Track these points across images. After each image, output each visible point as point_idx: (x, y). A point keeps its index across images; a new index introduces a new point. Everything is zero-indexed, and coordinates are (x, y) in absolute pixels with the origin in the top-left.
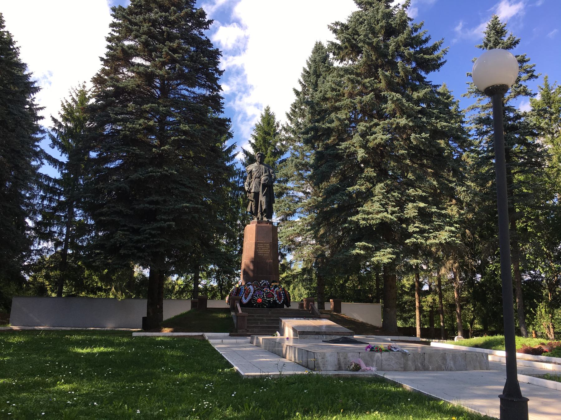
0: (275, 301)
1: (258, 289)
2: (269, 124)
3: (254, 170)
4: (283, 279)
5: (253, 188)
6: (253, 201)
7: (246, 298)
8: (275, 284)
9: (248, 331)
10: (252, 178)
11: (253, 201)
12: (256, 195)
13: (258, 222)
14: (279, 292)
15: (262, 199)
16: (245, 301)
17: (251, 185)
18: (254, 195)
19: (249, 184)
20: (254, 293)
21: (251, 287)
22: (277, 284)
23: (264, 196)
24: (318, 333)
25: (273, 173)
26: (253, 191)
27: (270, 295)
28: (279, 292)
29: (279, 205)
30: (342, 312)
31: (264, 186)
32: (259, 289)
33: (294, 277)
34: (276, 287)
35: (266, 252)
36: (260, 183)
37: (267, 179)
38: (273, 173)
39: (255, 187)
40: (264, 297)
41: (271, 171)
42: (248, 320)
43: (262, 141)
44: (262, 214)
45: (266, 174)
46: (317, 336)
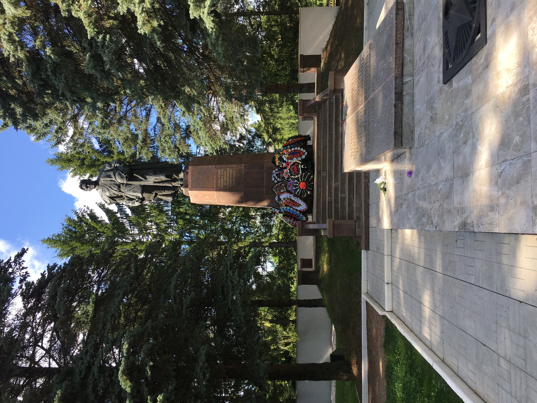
0: (303, 161)
1: (286, 186)
2: (69, 161)
3: (108, 194)
4: (270, 137)
5: (135, 194)
6: (156, 194)
7: (299, 205)
8: (277, 160)
9: (359, 218)
10: (122, 196)
11: (156, 194)
12: (145, 189)
13: (186, 186)
14: (290, 154)
15: (151, 180)
16: (303, 206)
17: (132, 197)
18: (146, 192)
19: (131, 199)
20: (291, 193)
21: (282, 197)
22: (277, 156)
23: (146, 179)
24: (399, 96)
25: (111, 166)
26: (140, 195)
27: (294, 168)
28: (290, 154)
29: (167, 151)
30: (319, 52)
31: (131, 178)
32: (284, 184)
33: (267, 124)
34: (281, 159)
35: (227, 173)
36: (127, 184)
37: (120, 175)
38: (111, 166)
39: (134, 192)
40: (298, 179)
41: (108, 168)
42: (337, 218)
43: (93, 169)
44: (175, 180)
45: (113, 176)
46: (407, 99)
